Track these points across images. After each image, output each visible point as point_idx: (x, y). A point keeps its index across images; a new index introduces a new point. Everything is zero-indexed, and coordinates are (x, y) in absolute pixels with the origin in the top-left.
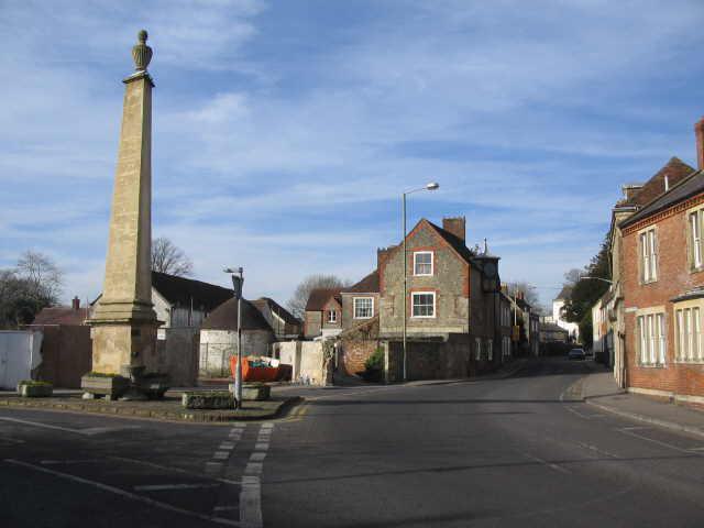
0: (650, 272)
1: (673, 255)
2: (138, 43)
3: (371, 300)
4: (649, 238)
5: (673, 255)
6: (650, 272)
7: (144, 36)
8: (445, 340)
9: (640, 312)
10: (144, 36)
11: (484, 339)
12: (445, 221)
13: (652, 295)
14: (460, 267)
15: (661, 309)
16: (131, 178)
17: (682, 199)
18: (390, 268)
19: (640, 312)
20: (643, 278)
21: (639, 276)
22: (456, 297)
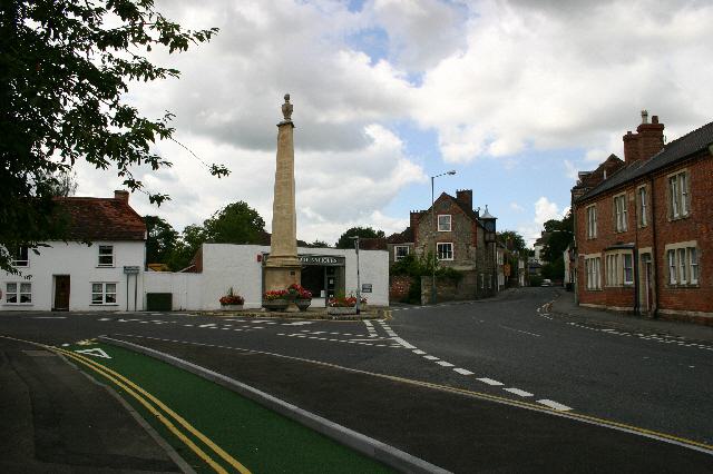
0: (593, 233)
1: (607, 223)
2: (284, 102)
3: (407, 246)
4: (593, 212)
5: (607, 223)
6: (593, 233)
7: (287, 98)
8: (622, 157)
9: (587, 257)
10: (287, 98)
11: (486, 274)
12: (457, 192)
13: (593, 245)
14: (468, 225)
15: (599, 255)
16: (307, 187)
17: (657, 169)
18: (422, 226)
19: (587, 257)
20: (642, 223)
21: (639, 220)
22: (468, 246)
